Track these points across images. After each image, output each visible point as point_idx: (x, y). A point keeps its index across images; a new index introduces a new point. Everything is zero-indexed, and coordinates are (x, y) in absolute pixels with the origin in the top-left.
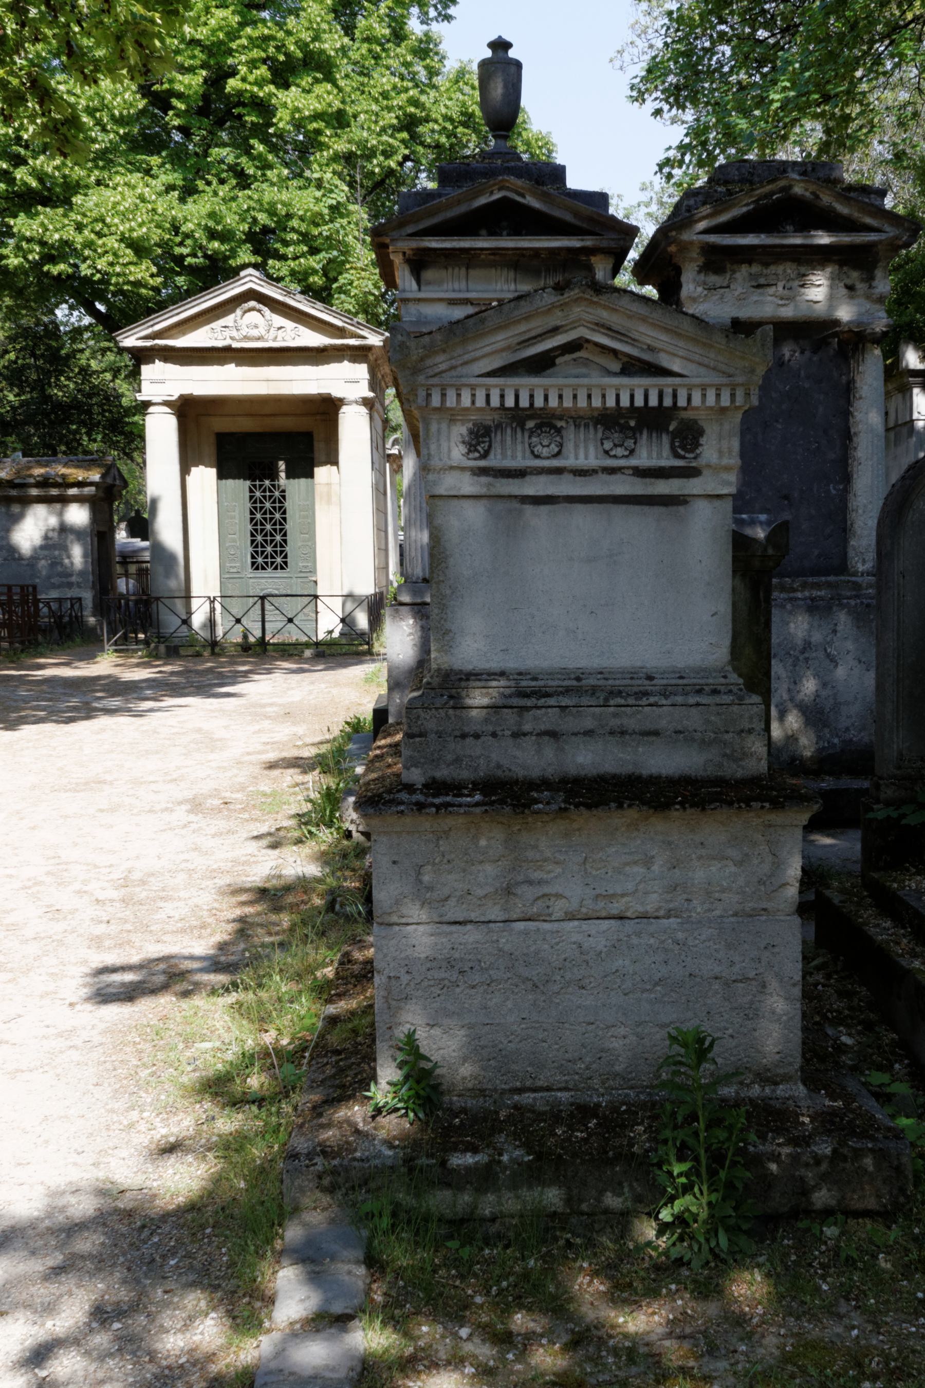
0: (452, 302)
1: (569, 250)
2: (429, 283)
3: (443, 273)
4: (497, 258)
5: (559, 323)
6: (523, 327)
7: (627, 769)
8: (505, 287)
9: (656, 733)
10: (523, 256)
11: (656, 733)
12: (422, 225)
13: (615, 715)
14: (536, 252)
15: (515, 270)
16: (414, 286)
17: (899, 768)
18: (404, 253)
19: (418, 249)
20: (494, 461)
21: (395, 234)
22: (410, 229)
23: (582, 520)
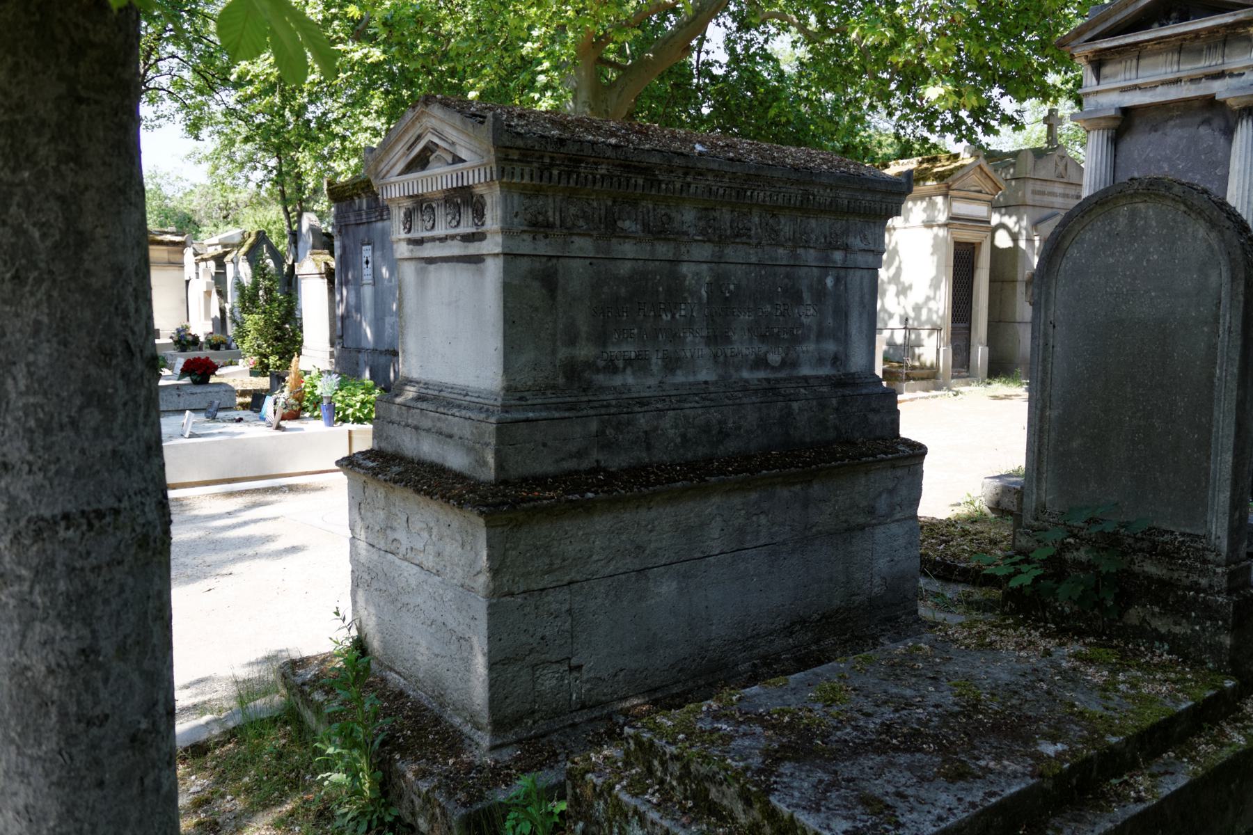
0: (1124, 90)
1: (1226, 26)
2: (1106, 77)
3: (1120, 67)
4: (1162, 46)
5: (419, 132)
6: (406, 139)
7: (438, 460)
8: (1169, 70)
9: (451, 436)
10: (1185, 39)
11: (451, 436)
12: (1096, 32)
13: (439, 419)
14: (1197, 34)
15: (1180, 53)
16: (1094, 81)
17: (1037, 519)
18: (1086, 57)
19: (1096, 51)
20: (416, 234)
21: (1074, 43)
22: (1087, 37)
23: (445, 271)
